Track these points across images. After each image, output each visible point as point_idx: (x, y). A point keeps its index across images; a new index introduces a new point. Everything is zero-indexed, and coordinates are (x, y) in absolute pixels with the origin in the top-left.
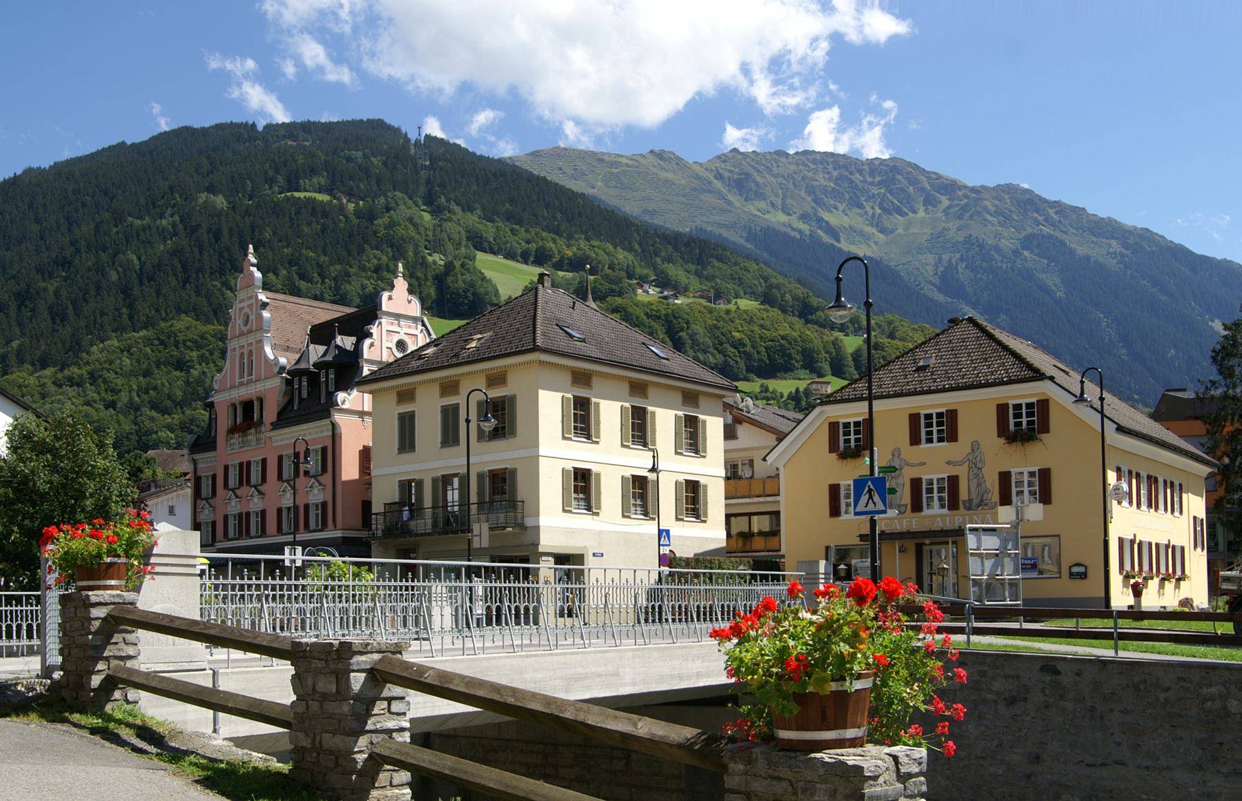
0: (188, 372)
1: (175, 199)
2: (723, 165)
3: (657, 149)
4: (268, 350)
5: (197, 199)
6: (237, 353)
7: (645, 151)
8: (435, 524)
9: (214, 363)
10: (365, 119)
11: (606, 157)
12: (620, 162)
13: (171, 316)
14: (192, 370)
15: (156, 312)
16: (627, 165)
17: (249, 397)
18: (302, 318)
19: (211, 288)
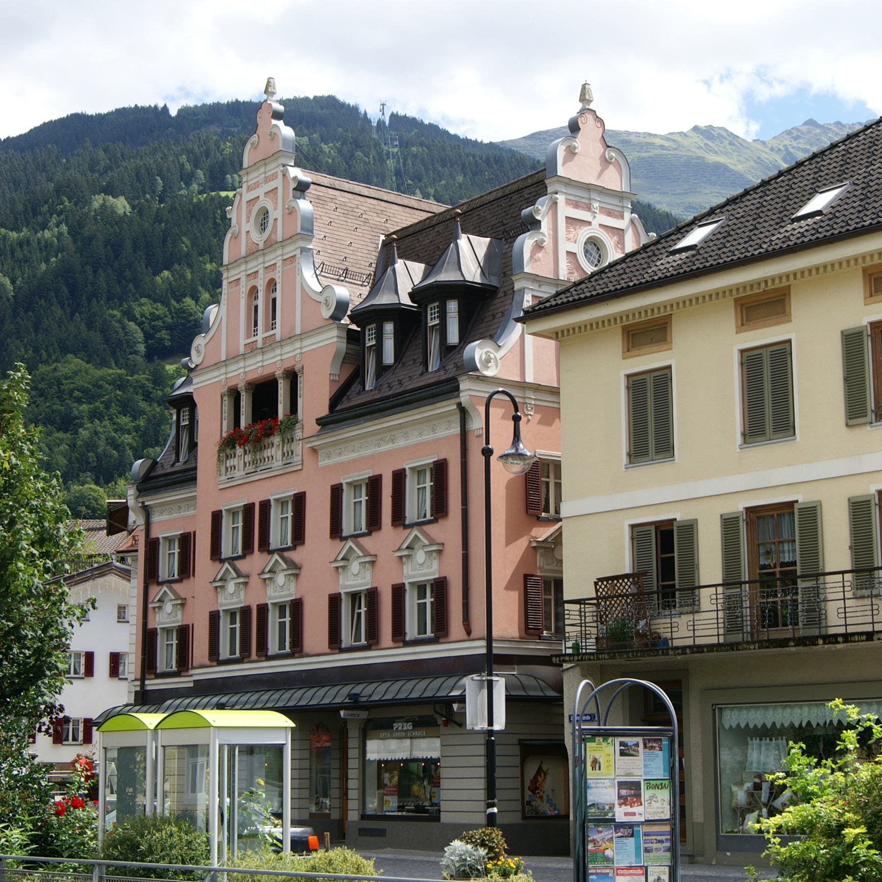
0: (76, 433)
1: (62, 203)
2: (794, 144)
3: (702, 124)
4: (308, 275)
5: (91, 203)
6: (244, 289)
7: (686, 128)
8: (732, 622)
9: (111, 419)
10: (311, 97)
11: (633, 139)
12: (653, 144)
13: (53, 357)
14: (80, 430)
15: (34, 352)
16: (662, 147)
17: (267, 371)
18: (366, 221)
19: (108, 318)
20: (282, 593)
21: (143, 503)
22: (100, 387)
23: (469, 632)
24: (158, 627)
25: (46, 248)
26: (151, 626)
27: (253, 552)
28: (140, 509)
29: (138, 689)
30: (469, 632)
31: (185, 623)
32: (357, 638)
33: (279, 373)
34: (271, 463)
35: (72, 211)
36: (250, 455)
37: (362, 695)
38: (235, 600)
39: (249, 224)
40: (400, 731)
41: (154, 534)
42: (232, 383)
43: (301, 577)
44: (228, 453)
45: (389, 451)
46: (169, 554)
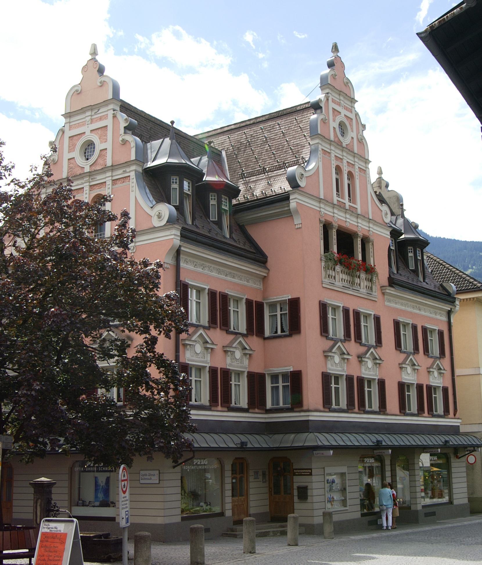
17: (355, 229)
23: (455, 415)
30: (455, 415)
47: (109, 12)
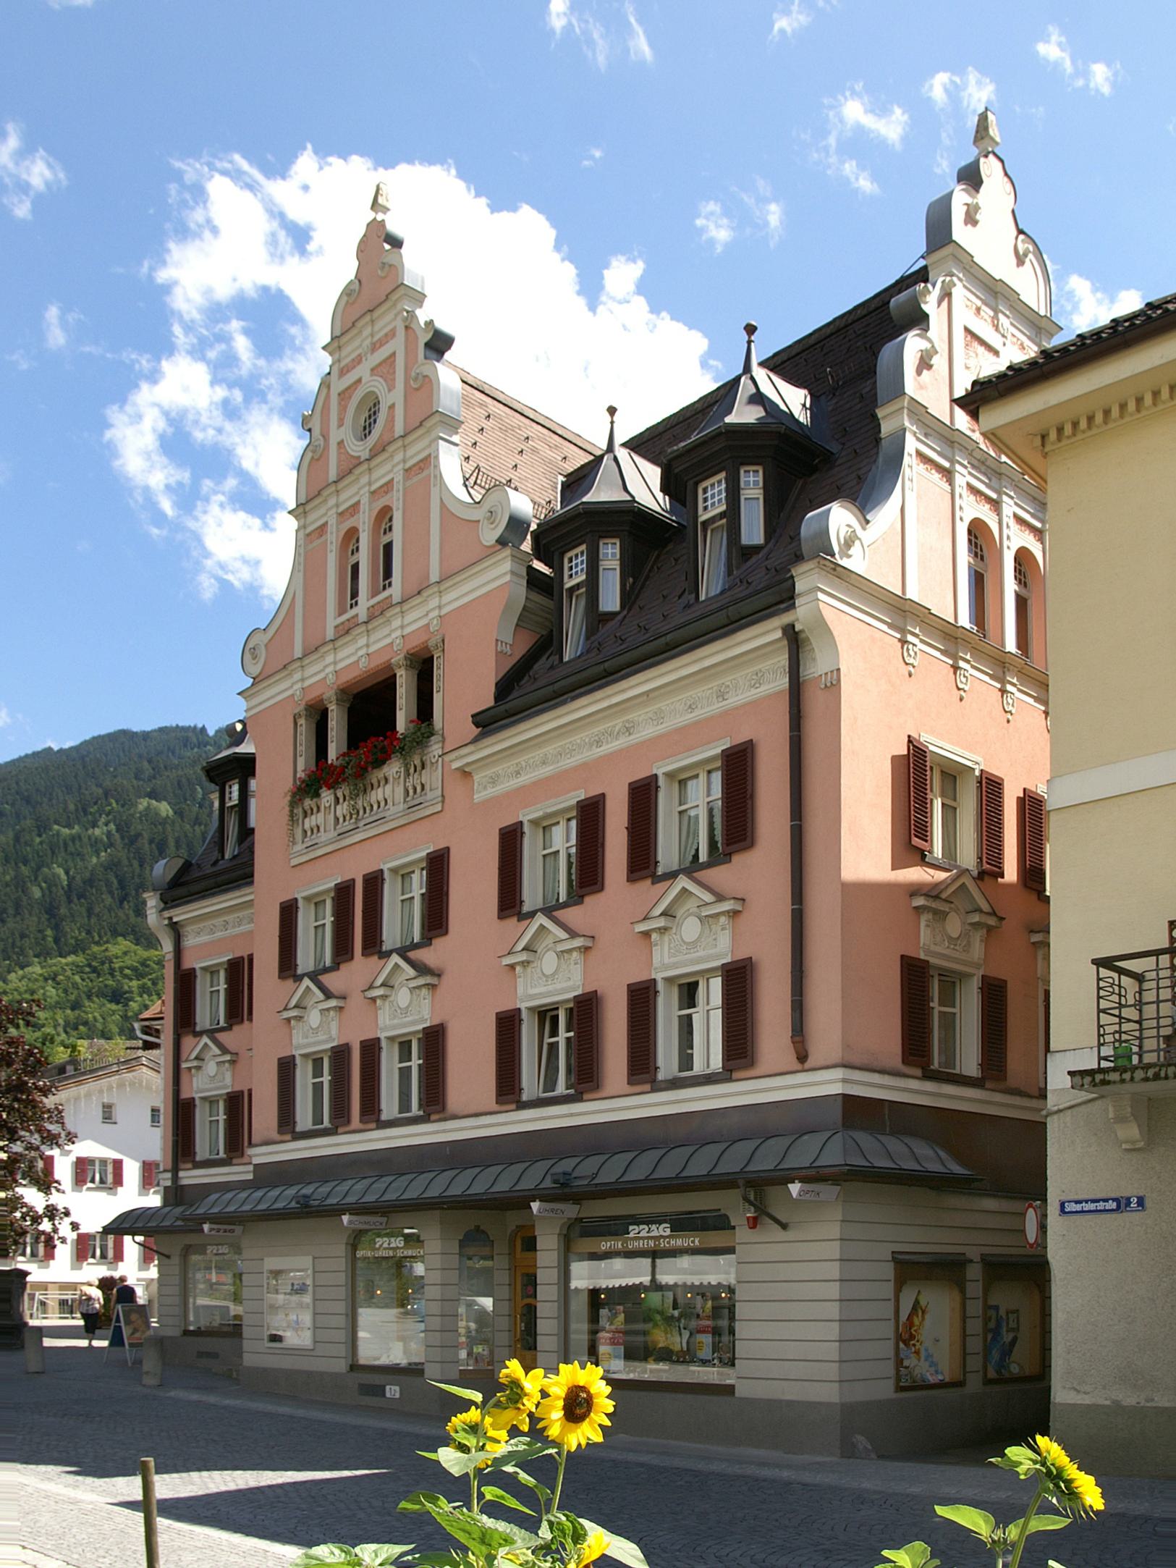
0: (126, 1005)
1: (110, 804)
14: (131, 1003)
17: (378, 662)
20: (407, 1019)
21: (170, 918)
22: (148, 966)
23: (802, 1057)
24: (197, 1096)
25: (95, 844)
26: (185, 1095)
27: (352, 958)
28: (167, 929)
29: (169, 1183)
30: (802, 1057)
31: (237, 1088)
32: (550, 1083)
33: (398, 658)
34: (384, 810)
35: (119, 812)
36: (346, 803)
37: (573, 1175)
38: (322, 1037)
39: (343, 429)
40: (385, 1249)
41: (187, 964)
42: (312, 695)
43: (439, 991)
44: (307, 808)
45: (621, 751)
46: (212, 992)
47: (514, 209)
